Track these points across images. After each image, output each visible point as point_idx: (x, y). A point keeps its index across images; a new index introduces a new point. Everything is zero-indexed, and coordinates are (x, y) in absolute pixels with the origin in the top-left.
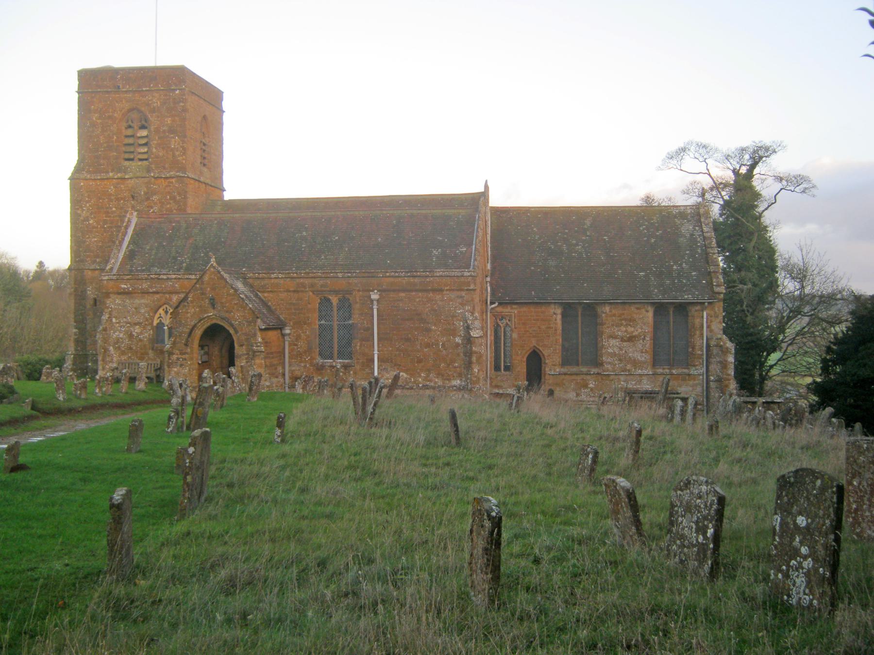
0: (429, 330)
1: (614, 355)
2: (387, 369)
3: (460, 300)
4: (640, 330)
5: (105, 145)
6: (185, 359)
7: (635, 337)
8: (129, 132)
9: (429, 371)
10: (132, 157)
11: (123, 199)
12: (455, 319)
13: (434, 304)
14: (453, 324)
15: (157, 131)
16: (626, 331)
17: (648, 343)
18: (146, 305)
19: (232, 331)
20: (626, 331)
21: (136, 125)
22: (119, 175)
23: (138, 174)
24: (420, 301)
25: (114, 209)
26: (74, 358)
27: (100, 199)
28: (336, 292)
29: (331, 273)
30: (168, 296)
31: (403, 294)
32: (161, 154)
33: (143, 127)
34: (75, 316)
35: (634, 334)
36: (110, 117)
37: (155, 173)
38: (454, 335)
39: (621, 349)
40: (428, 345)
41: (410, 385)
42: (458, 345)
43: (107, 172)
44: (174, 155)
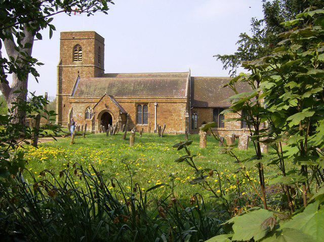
0: (172, 115)
8: (76, 52)
11: (74, 73)
15: (85, 51)
19: (111, 114)
21: (78, 49)
23: (79, 65)
28: (143, 103)
33: (81, 50)
36: (70, 47)
40: (172, 120)
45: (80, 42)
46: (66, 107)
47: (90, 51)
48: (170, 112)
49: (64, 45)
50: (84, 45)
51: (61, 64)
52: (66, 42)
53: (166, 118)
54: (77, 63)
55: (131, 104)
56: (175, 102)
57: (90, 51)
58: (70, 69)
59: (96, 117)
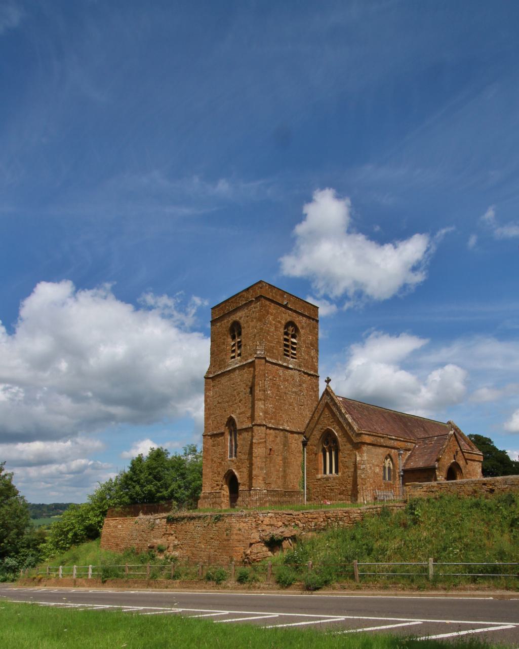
5: (277, 340)
15: (304, 341)
27: (275, 377)
32: (306, 357)
58: (281, 371)
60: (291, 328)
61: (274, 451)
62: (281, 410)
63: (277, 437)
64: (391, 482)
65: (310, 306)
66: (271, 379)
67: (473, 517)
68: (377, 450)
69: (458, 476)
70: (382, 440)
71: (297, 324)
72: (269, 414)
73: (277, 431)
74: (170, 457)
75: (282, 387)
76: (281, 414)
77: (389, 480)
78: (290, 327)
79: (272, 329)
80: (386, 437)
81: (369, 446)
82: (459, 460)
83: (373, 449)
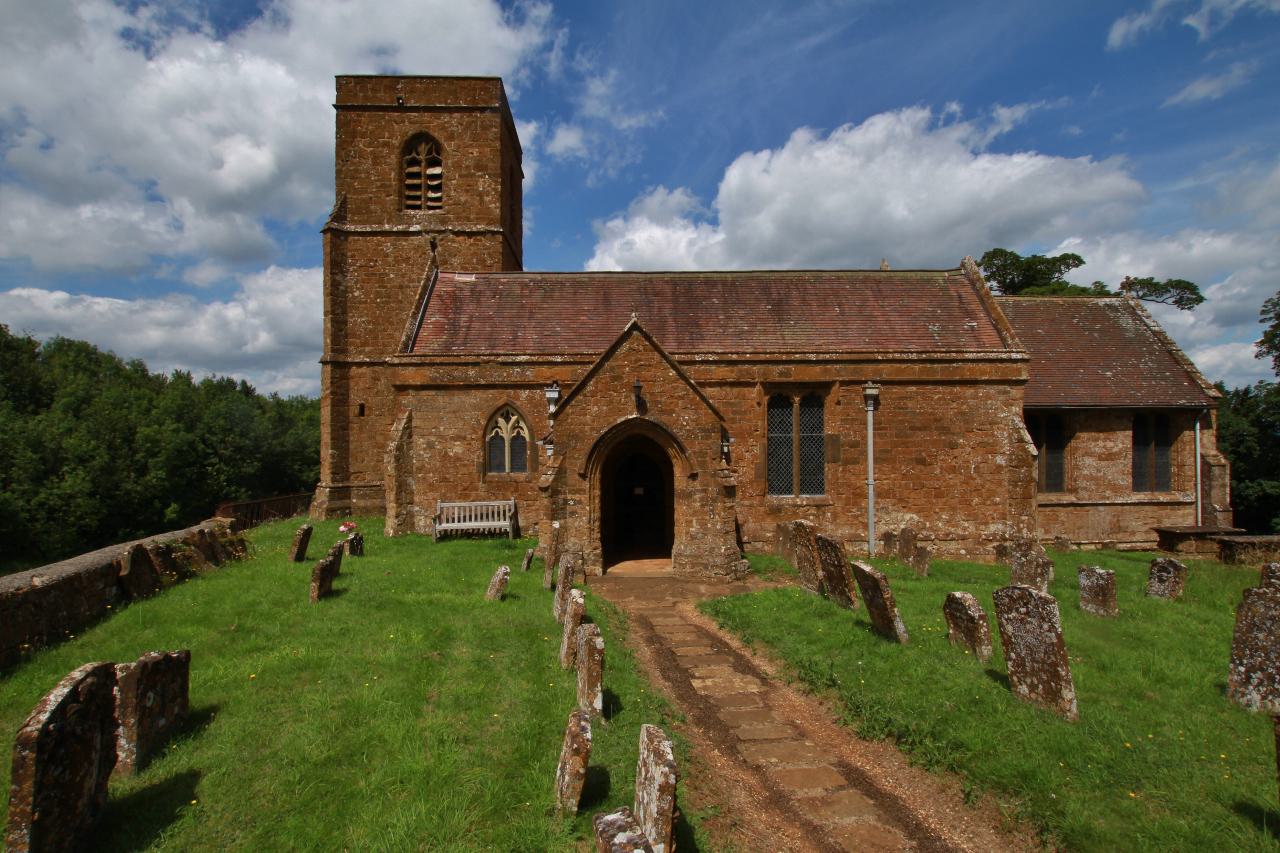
0: (953, 446)
1: (1091, 478)
2: (887, 509)
3: (1002, 398)
4: (1121, 446)
5: (378, 184)
6: (580, 502)
7: (1115, 454)
9: (954, 509)
10: (419, 203)
12: (995, 427)
13: (963, 404)
14: (993, 435)
15: (457, 166)
16: (1104, 447)
17: (1126, 463)
18: (475, 407)
20: (1104, 447)
22: (400, 227)
24: (939, 399)
25: (392, 276)
26: (330, 492)
27: (370, 261)
29: (797, 353)
30: (512, 392)
31: (914, 388)
32: (463, 199)
33: (437, 163)
34: (332, 430)
35: (1114, 450)
36: (386, 144)
37: (454, 226)
38: (994, 453)
39: (1099, 471)
40: (953, 470)
41: (925, 533)
42: (1000, 467)
43: (381, 223)
44: (482, 201)
45: (434, 125)
46: (371, 418)
47: (479, 167)
48: (945, 430)
49: (354, 135)
50: (451, 137)
51: (339, 215)
52: (366, 122)
53: (921, 462)
54: (418, 221)
55: (736, 390)
56: (968, 375)
57: (479, 167)
58: (388, 246)
59: (578, 462)
60: (423, 148)
61: (370, 408)
62: (391, 323)
63: (379, 380)
64: (522, 476)
65: (473, 82)
66: (361, 266)
67: (1028, 626)
68: (456, 399)
69: (674, 461)
70: (472, 372)
71: (436, 135)
72: (359, 337)
73: (376, 368)
74: (1153, 445)
75: (392, 276)
76: (389, 331)
77: (513, 469)
78: (423, 145)
79: (367, 164)
80: (488, 362)
81: (424, 393)
82: (670, 412)
83: (440, 398)
